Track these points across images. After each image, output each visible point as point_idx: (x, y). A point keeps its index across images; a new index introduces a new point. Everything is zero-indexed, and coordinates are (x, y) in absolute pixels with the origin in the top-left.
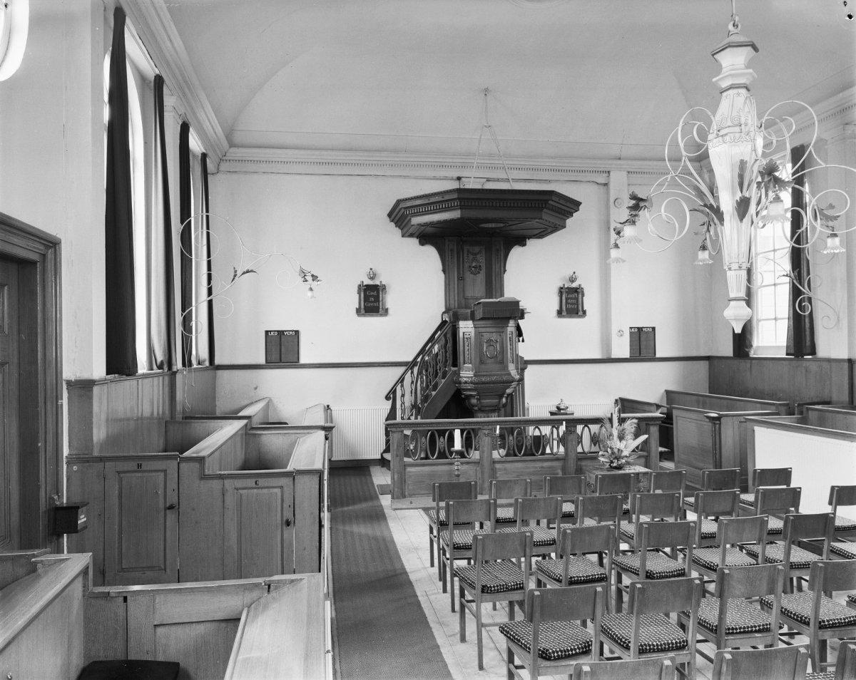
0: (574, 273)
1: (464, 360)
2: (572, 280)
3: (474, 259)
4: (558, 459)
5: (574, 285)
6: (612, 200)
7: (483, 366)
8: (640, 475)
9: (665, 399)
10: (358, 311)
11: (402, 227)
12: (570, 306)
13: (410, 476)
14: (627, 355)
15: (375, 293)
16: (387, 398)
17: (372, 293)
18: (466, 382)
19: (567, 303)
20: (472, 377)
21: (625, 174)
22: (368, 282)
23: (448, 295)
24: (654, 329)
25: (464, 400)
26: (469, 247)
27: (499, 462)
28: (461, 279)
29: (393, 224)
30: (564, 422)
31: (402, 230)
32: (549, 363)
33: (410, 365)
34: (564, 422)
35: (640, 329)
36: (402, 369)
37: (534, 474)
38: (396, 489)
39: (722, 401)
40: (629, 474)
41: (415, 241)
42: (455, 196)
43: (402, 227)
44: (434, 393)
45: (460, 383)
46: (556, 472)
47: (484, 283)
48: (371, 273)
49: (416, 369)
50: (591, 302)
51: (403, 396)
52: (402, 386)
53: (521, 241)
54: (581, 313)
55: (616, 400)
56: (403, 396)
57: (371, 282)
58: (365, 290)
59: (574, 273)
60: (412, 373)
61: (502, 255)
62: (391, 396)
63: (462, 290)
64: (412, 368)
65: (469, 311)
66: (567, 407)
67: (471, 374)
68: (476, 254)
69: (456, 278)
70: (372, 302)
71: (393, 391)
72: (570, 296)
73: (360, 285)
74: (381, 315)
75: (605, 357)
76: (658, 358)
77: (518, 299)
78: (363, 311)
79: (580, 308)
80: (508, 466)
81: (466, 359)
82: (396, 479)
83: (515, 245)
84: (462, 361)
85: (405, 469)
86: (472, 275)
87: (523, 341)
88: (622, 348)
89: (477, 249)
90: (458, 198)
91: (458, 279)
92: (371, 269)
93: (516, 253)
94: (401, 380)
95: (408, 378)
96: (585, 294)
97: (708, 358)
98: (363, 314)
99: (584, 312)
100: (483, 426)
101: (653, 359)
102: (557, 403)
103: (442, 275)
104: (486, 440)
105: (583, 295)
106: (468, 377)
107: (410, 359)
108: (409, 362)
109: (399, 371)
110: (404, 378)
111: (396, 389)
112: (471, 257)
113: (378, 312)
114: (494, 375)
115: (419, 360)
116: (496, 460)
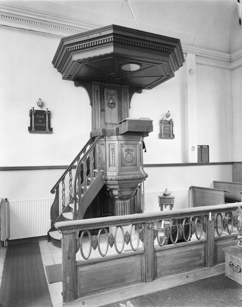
0: (169, 111)
2: (168, 116)
3: (111, 98)
4: (201, 243)
5: (168, 119)
7: (123, 168)
9: (213, 185)
10: (30, 129)
11: (62, 72)
12: (166, 132)
13: (82, 276)
14: (195, 160)
15: (43, 117)
16: (52, 192)
17: (40, 117)
19: (164, 130)
20: (116, 176)
21: (195, 56)
22: (37, 108)
24: (208, 146)
25: (108, 191)
26: (107, 90)
27: (159, 251)
29: (56, 70)
31: (62, 74)
32: (155, 166)
33: (69, 169)
35: (201, 147)
36: (63, 171)
38: (68, 292)
39: (236, 185)
41: (72, 83)
42: (111, 31)
43: (62, 72)
44: (88, 187)
47: (117, 114)
48: (40, 102)
49: (74, 172)
50: (177, 130)
51: (64, 190)
52: (63, 183)
53: (139, 89)
54: (172, 136)
55: (190, 188)
56: (64, 190)
57: (39, 109)
58: (35, 114)
59: (169, 111)
61: (128, 97)
62: (55, 190)
64: (70, 170)
66: (170, 194)
67: (115, 174)
68: (113, 95)
69: (99, 110)
70: (40, 123)
71: (57, 187)
72: (166, 126)
73: (31, 110)
74: (47, 133)
75: (184, 163)
77: (151, 119)
78: (33, 129)
79: (171, 133)
80: (166, 253)
82: (68, 282)
83: (135, 92)
85: (77, 269)
86: (110, 109)
87: (145, 151)
88: (193, 157)
89: (112, 92)
90: (113, 34)
92: (40, 99)
93: (136, 97)
94: (62, 178)
95: (67, 177)
96: (174, 125)
97: (232, 163)
98: (34, 132)
99: (174, 136)
100: (147, 220)
101: (208, 163)
102: (163, 191)
104: (150, 233)
107: (69, 164)
108: (68, 166)
110: (64, 177)
111: (59, 185)
112: (109, 96)
115: (76, 164)
116: (157, 249)
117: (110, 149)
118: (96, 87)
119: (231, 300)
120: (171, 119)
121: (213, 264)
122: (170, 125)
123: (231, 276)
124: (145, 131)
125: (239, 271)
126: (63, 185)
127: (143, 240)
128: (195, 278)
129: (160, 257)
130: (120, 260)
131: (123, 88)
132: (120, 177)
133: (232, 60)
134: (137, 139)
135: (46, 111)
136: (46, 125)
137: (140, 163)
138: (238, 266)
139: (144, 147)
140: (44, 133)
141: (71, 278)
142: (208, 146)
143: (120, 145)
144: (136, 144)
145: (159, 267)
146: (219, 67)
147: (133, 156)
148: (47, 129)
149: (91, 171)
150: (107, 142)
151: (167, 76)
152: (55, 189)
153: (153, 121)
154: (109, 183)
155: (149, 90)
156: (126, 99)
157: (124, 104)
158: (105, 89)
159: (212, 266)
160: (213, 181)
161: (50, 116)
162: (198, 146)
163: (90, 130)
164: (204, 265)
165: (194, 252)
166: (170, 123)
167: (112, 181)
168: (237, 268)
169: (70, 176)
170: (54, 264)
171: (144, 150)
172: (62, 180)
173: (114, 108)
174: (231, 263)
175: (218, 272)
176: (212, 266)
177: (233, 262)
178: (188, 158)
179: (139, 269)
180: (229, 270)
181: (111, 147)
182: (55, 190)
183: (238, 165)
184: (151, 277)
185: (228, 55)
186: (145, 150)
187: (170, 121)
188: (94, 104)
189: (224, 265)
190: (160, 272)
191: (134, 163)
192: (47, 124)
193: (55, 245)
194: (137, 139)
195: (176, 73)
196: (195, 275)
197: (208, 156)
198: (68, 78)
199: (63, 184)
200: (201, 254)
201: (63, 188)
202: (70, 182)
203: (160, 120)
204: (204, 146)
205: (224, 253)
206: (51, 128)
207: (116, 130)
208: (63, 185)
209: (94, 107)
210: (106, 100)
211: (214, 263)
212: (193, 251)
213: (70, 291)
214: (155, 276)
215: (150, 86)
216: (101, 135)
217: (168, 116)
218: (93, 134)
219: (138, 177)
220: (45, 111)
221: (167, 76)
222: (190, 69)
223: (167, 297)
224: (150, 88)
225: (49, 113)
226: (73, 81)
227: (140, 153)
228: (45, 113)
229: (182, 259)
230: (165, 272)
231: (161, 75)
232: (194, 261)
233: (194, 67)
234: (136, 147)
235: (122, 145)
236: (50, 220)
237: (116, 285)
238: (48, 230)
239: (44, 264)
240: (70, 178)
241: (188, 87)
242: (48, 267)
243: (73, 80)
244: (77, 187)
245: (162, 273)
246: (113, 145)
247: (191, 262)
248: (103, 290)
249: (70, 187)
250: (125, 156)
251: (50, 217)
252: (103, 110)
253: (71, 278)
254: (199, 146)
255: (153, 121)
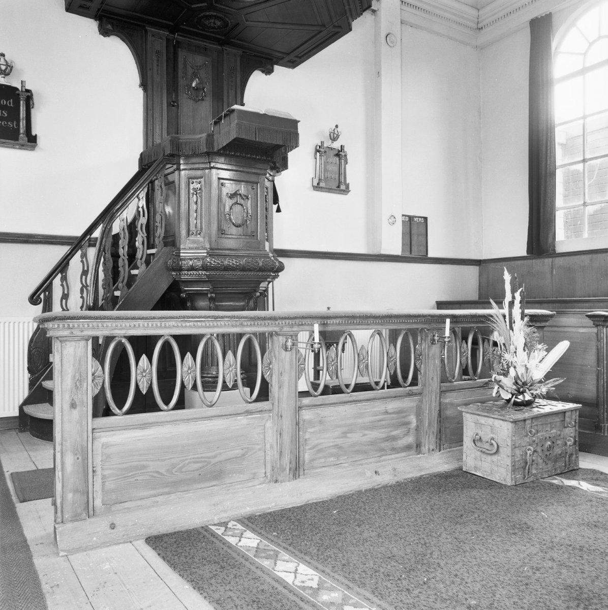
0: (337, 126)
1: (188, 231)
5: (336, 145)
6: (383, 35)
8: (568, 414)
16: (34, 299)
18: (192, 268)
20: (203, 258)
23: (150, 127)
24: (426, 219)
28: (173, 104)
30: (448, 321)
33: (77, 244)
34: (448, 321)
35: (411, 218)
36: (64, 250)
37: (372, 426)
40: (579, 420)
41: (91, 25)
45: (180, 269)
46: (406, 420)
49: (92, 252)
50: (354, 172)
51: (65, 297)
52: (64, 279)
54: (343, 187)
56: (65, 297)
59: (337, 126)
60: (84, 255)
63: (174, 126)
65: (204, 135)
71: (46, 287)
74: (22, 147)
76: (431, 258)
81: (192, 228)
84: (184, 232)
87: (279, 210)
88: (393, 244)
89: (199, 60)
91: (169, 105)
94: (62, 267)
95: (76, 263)
99: (347, 186)
101: (424, 259)
103: (140, 93)
104: (288, 359)
105: (346, 162)
106: (197, 258)
107: (79, 233)
108: (76, 238)
109: (59, 252)
110: (68, 264)
111: (51, 283)
113: (16, 139)
114: (243, 257)
115: (97, 234)
117: (192, 191)
118: (157, 40)
119: (476, 506)
120: (341, 146)
121: (437, 446)
122: (339, 160)
123: (476, 468)
124: (281, 143)
125: (494, 451)
126: (64, 283)
127: (271, 376)
128: (395, 476)
129: (311, 423)
130: (212, 424)
131: (225, 56)
132: (213, 261)
133: (480, 26)
134: (258, 171)
135: (20, 89)
136: (18, 125)
137: (266, 234)
138: (492, 439)
139: (276, 200)
140: (13, 147)
141: (78, 459)
142: (426, 219)
143: (217, 181)
144: (257, 183)
145: (310, 449)
146: (451, 38)
147: (250, 212)
148: (21, 135)
149: (139, 254)
150: (183, 173)
151: (334, 26)
152: (40, 294)
153: (299, 121)
154: (186, 277)
155: (291, 69)
156: (232, 82)
157: (228, 93)
158: (180, 49)
159: (433, 450)
160: (436, 302)
161: (31, 103)
162: (403, 215)
163: (140, 149)
164: (418, 447)
165: (393, 415)
166: (340, 154)
167: (195, 272)
168: (492, 444)
169: (82, 261)
170: (35, 468)
171: (275, 207)
172: (61, 272)
173: (204, 103)
174: (478, 437)
175: (447, 463)
176: (433, 450)
177: (481, 434)
178: (381, 243)
179: (260, 449)
180: (473, 456)
181: (192, 186)
182: (42, 296)
183: (492, 265)
184: (290, 469)
185: (474, 12)
186: (278, 206)
187: (339, 151)
188: (150, 87)
189: (462, 449)
190: (312, 461)
191: (249, 230)
192: (21, 124)
193: (38, 437)
194: (258, 171)
195: (355, 24)
196: (395, 470)
197: (425, 250)
198: (81, 10)
199: (62, 282)
200: (408, 423)
201: (64, 292)
202: (84, 277)
203: (317, 146)
204: (416, 217)
205: (462, 416)
206: (33, 134)
207: (207, 140)
208: (62, 285)
209: (150, 92)
210: (183, 78)
211: (438, 445)
212: (390, 414)
213: (76, 491)
214: (297, 470)
215: (292, 57)
216: (168, 152)
217: (334, 137)
218: (147, 157)
219: (261, 264)
220: (16, 89)
221: (334, 26)
222: (388, 32)
223: (328, 510)
224: (293, 63)
225: (29, 94)
226: (96, 20)
227: (266, 209)
228: (17, 92)
229: (366, 432)
230: (323, 460)
231: (320, 24)
232: (394, 438)
233: (396, 29)
234: (256, 189)
235: (222, 181)
236: (27, 375)
237: (200, 487)
238: (21, 401)
239: (5, 470)
240: (82, 268)
241: (383, 73)
242: (15, 476)
243: (96, 17)
244: (101, 291)
245: (316, 463)
246: (198, 180)
247: (387, 439)
248: (167, 496)
249: (82, 291)
250: (227, 209)
251: (26, 365)
252: (173, 102)
253: (78, 459)
254: (406, 216)
255: (299, 121)
